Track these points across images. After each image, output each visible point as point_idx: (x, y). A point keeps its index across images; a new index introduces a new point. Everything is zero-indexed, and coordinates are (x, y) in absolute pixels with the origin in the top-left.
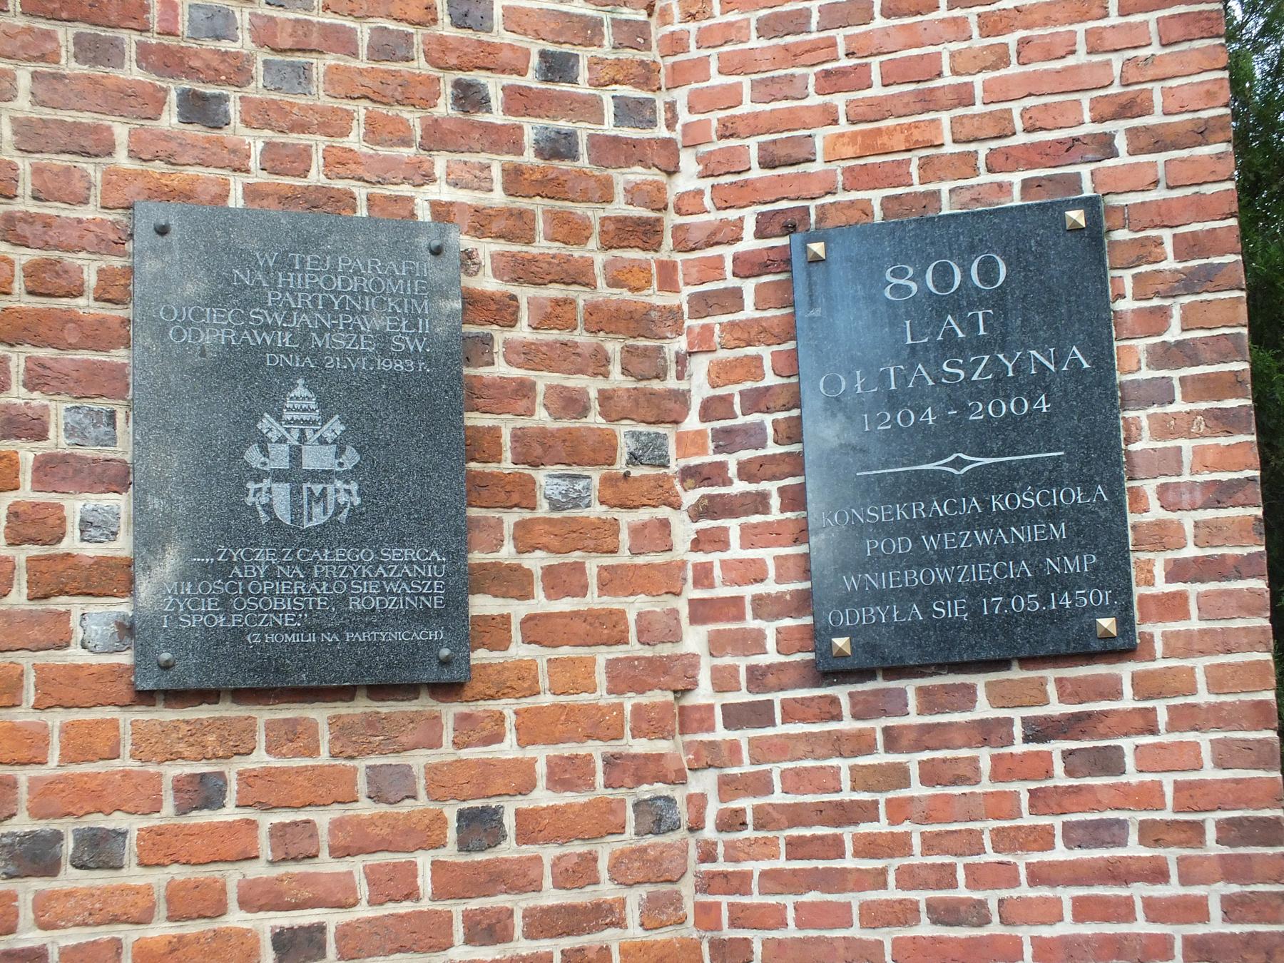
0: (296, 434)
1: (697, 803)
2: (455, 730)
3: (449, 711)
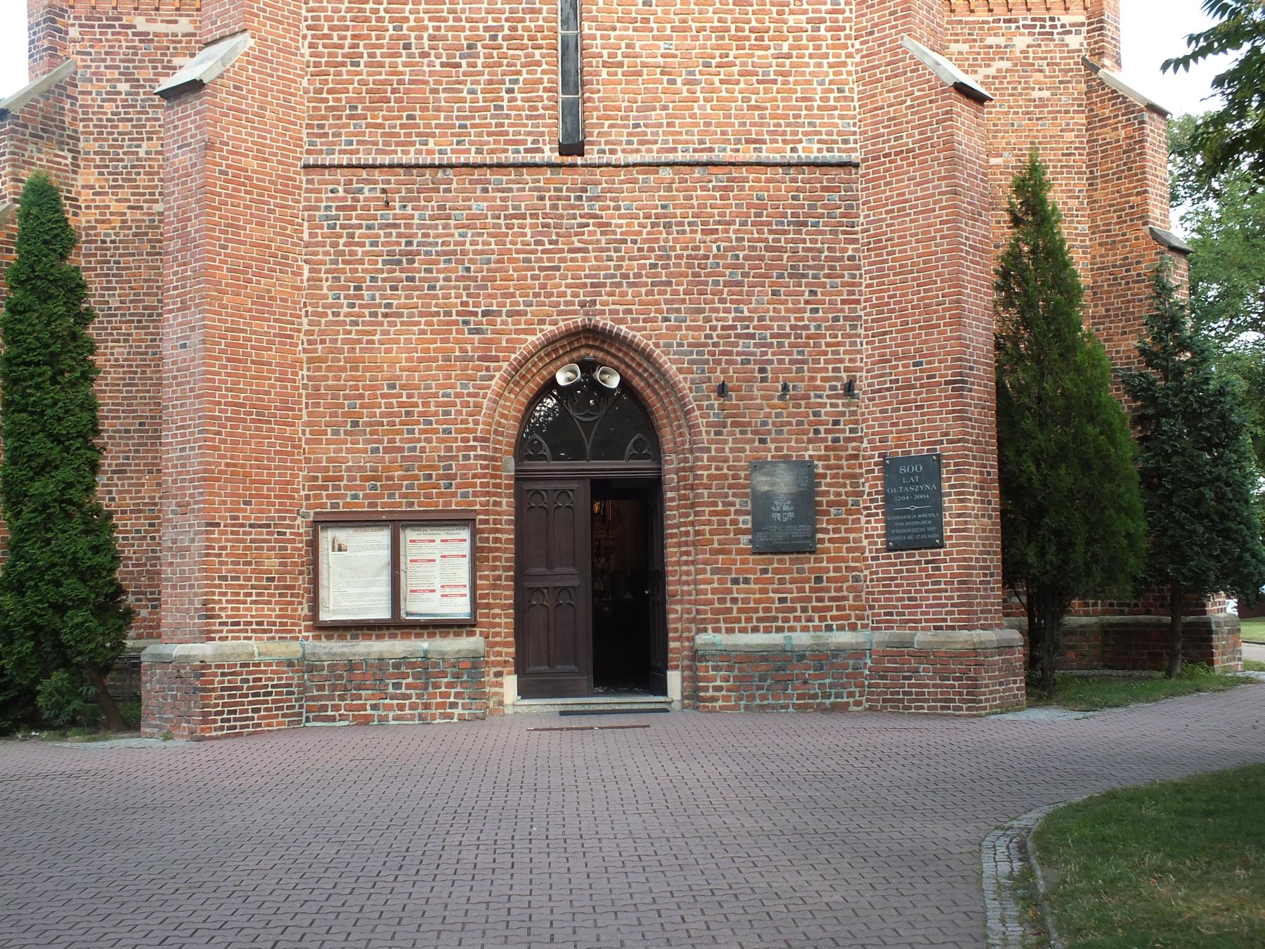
1: (865, 576)
3: (813, 557)
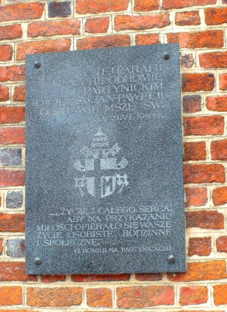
0: (97, 153)
2: (180, 296)
